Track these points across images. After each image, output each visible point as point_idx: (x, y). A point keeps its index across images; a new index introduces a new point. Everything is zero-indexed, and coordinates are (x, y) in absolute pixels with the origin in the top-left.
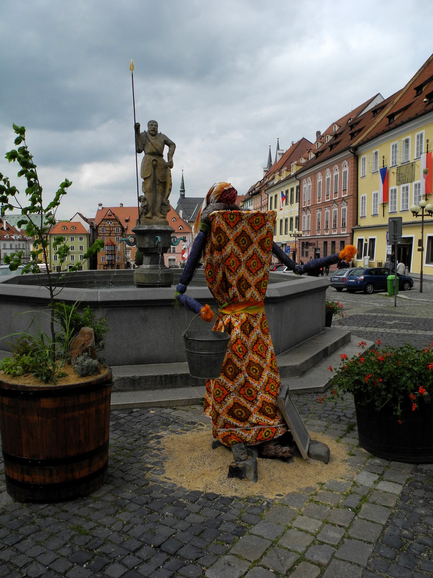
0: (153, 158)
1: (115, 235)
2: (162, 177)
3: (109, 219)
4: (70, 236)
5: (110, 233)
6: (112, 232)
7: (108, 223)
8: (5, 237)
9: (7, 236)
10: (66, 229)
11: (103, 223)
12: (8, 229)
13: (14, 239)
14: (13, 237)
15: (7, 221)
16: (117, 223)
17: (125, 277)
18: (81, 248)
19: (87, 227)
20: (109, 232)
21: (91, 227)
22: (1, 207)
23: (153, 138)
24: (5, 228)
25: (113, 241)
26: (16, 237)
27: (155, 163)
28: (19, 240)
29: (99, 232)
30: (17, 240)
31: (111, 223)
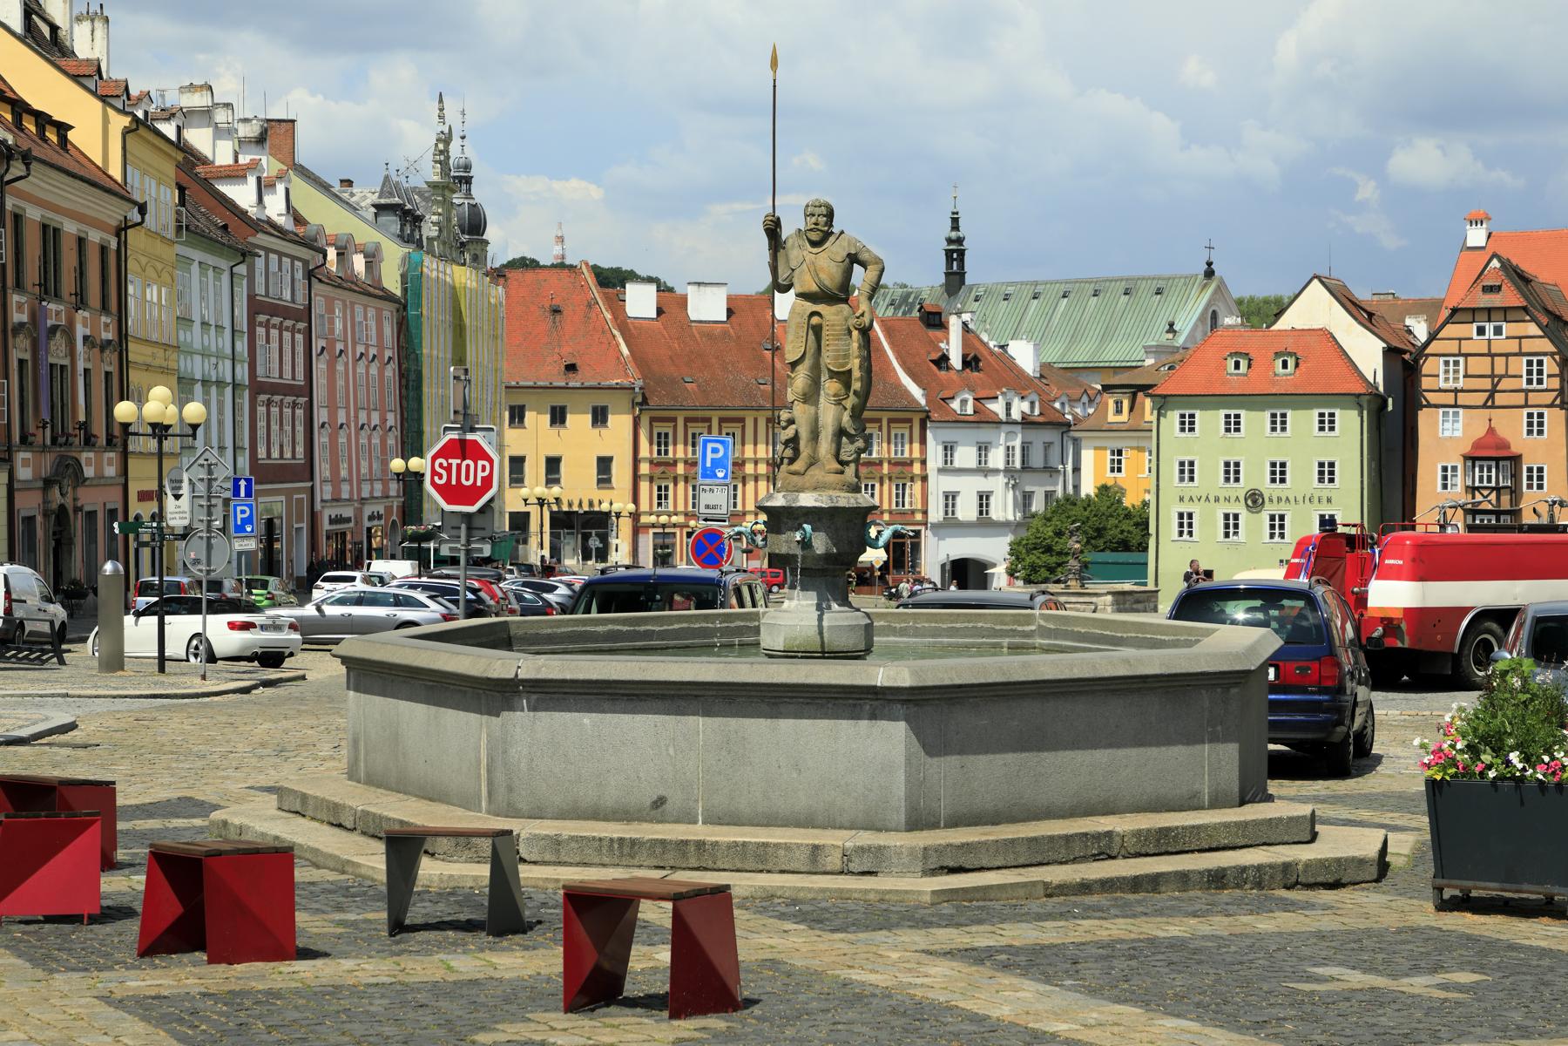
0: (810, 307)
1: (1519, 399)
2: (836, 358)
3: (1489, 312)
4: (1217, 407)
5: (1493, 392)
6: (1505, 384)
7: (1481, 331)
8: (955, 405)
9: (964, 402)
10: (1243, 364)
11: (1451, 330)
12: (970, 362)
13: (1003, 416)
14: (997, 407)
15: (966, 317)
16: (1533, 329)
17: (739, 631)
18: (1327, 472)
19: (1368, 353)
20: (1486, 384)
21: (1391, 353)
22: (950, 241)
23: (815, 250)
24: (956, 361)
25: (1503, 432)
26: (1008, 406)
27: (815, 320)
28: (1026, 422)
29: (1426, 383)
30: (1015, 423)
31: (1498, 331)
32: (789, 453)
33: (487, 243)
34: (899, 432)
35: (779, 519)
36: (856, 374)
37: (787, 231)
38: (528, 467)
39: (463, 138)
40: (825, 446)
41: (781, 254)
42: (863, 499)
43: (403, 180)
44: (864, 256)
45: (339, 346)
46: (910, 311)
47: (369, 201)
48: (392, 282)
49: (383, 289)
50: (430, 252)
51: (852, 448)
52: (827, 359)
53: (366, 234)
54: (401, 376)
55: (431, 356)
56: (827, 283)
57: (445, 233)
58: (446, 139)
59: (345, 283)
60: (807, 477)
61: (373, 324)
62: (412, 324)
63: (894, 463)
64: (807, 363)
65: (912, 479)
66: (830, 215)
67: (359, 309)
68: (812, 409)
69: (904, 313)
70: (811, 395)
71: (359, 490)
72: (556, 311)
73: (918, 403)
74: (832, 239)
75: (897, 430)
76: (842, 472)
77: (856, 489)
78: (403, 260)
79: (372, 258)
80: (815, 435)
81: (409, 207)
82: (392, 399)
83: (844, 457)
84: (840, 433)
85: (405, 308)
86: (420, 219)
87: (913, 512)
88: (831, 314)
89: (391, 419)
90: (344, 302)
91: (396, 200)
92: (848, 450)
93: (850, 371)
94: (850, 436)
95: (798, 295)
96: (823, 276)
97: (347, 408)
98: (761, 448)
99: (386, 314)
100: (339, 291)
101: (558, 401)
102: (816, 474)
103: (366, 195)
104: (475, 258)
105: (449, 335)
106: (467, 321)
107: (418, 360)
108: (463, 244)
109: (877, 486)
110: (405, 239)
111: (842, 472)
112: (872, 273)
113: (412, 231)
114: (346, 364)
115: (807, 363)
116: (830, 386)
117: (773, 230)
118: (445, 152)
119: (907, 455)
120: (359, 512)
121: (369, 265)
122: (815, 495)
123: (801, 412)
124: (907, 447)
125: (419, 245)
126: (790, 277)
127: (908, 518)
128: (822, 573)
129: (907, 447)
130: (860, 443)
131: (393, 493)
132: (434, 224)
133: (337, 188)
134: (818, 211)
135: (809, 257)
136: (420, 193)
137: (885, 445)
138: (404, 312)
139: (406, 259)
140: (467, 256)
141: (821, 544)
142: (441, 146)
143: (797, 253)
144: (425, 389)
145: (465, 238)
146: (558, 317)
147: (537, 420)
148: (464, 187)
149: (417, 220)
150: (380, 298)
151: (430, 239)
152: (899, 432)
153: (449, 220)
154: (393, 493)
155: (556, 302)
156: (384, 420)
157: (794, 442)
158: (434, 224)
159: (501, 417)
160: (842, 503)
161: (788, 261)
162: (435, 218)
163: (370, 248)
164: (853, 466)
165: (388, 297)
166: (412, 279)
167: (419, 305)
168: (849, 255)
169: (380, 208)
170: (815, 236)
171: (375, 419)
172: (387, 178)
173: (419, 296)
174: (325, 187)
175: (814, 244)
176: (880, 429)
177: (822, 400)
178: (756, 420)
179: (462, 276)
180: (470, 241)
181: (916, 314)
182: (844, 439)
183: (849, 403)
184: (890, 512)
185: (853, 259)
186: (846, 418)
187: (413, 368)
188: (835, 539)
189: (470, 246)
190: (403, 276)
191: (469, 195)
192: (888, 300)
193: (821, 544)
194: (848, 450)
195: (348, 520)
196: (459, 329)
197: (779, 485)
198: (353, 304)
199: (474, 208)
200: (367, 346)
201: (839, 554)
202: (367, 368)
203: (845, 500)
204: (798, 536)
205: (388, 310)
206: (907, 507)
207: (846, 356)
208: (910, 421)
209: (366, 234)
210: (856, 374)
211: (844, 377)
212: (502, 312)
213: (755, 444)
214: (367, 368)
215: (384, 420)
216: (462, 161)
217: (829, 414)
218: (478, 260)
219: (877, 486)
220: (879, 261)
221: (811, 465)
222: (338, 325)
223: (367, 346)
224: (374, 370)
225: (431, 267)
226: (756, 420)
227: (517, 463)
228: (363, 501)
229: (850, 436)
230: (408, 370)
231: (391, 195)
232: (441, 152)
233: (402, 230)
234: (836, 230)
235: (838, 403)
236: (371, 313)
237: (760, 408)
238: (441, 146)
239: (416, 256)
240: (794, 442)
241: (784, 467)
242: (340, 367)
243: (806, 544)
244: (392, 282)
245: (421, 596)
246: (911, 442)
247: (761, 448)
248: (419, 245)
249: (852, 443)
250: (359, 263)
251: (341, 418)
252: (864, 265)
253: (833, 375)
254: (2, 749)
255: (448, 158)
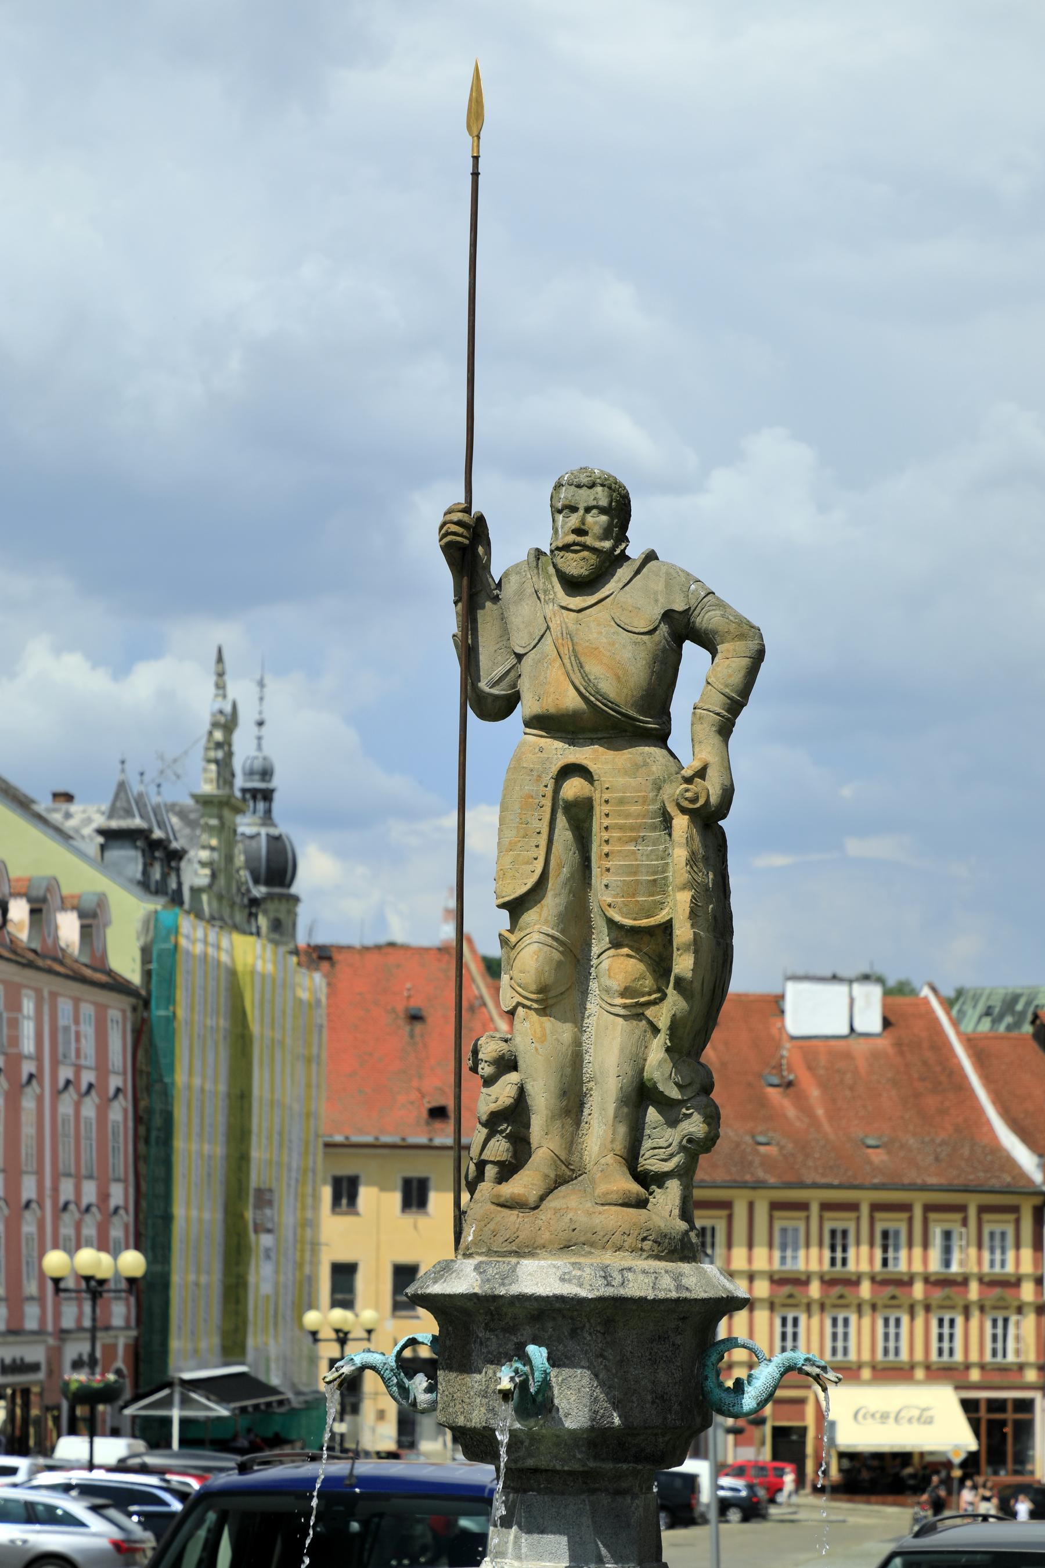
0: (560, 752)
2: (631, 890)
27: (574, 787)
32: (499, 1148)
33: (295, 899)
34: (998, 1228)
35: (473, 1329)
36: (683, 933)
37: (504, 557)
38: (361, 1281)
39: (260, 724)
40: (600, 1132)
41: (487, 615)
42: (702, 1280)
43: (152, 790)
44: (708, 619)
45: (28, 1067)
46: (1017, 1024)
47: (94, 825)
48: (125, 962)
49: (110, 973)
50: (197, 913)
51: (673, 1136)
52: (607, 895)
53: (80, 875)
54: (138, 1120)
55: (189, 1087)
56: (608, 687)
57: (222, 881)
58: (228, 723)
59: (42, 960)
60: (545, 1214)
61: (88, 1030)
62: (158, 1032)
63: (989, 1283)
64: (552, 904)
65: (1020, 1310)
66: (619, 510)
67: (65, 1006)
68: (565, 1032)
69: (1009, 1028)
70: (562, 993)
71: (57, 1315)
72: (415, 1018)
73: (1030, 1181)
74: (623, 573)
75: (994, 1224)
76: (641, 1204)
77: (685, 1249)
78: (146, 923)
79: (92, 920)
80: (572, 1102)
81: (158, 834)
82: (121, 1161)
83: (650, 1163)
84: (641, 1096)
85: (147, 1003)
86: (178, 855)
87: (1021, 1367)
88: (616, 771)
89: (117, 1194)
90: (38, 992)
91: (137, 822)
92: (663, 1142)
93: (667, 927)
94: (666, 1105)
95: (528, 724)
96: (595, 669)
97: (40, 1173)
98: (761, 1253)
99: (114, 1014)
100: (29, 973)
101: (416, 1171)
102: (571, 1206)
103: (89, 816)
104: (277, 926)
105: (223, 1053)
106: (255, 1028)
107: (167, 1094)
108: (254, 902)
109: (959, 1321)
110: (146, 886)
111: (641, 1204)
112: (731, 662)
113: (165, 876)
114: (40, 1099)
115: (552, 904)
116: (615, 968)
117: (466, 547)
118: (225, 746)
119: (1010, 1268)
120: (55, 1356)
121: (87, 932)
122: (562, 1263)
123: (536, 1039)
124: (1010, 1255)
125: (176, 899)
126: (512, 675)
127: (1012, 1378)
128: (585, 1482)
129: (1010, 1255)
130: (694, 1125)
131: (117, 1321)
132: (203, 864)
133: (43, 804)
134: (585, 497)
135: (560, 621)
136: (182, 814)
137: (973, 1251)
138: (144, 1012)
139: (151, 922)
140: (263, 921)
141: (577, 1400)
142: (218, 735)
143: (535, 611)
144: (179, 1144)
145: (260, 891)
146: (418, 1027)
147: (379, 1201)
148: (261, 806)
149: (173, 857)
150: (103, 986)
151: (196, 891)
152: (998, 1228)
153: (229, 858)
154: (117, 1321)
155: (416, 1003)
156: (104, 1196)
157: (513, 1118)
158: (203, 864)
159: (316, 1197)
160: (638, 1287)
161: (505, 633)
162: (204, 855)
163: (89, 904)
164: (674, 1186)
165: (118, 985)
166: (160, 956)
167: (170, 1000)
168: (668, 616)
169: (111, 837)
170: (576, 565)
171: (90, 1192)
172: (122, 786)
173: (169, 982)
174: (22, 803)
175: (574, 585)
176: (965, 1223)
177: (593, 1006)
178: (751, 1206)
179: (249, 953)
180: (269, 897)
181: (1028, 1029)
182: (652, 1114)
183: (662, 1015)
184: (982, 1367)
185: (681, 628)
186: (656, 1053)
187: (158, 1106)
188: (616, 1387)
189: (271, 906)
190: (146, 953)
191: (268, 818)
192: (981, 1008)
193: (577, 1400)
194: (663, 1142)
195: (35, 1367)
196: (241, 1042)
197: (469, 1236)
198: (54, 996)
199: (276, 842)
200: (78, 1069)
201: (628, 1428)
202: (77, 1106)
203: (648, 1279)
204: (505, 1378)
205: (117, 1010)
206: (1011, 1358)
207: (658, 886)
208: (1015, 1209)
209: (80, 875)
210: (683, 933)
211: (652, 943)
212: (321, 1016)
213: (750, 1245)
214: (77, 1106)
215: (104, 1196)
216: (258, 765)
217: (611, 1046)
218: (282, 928)
219: (959, 1321)
220: (749, 632)
221: (559, 1182)
222: (28, 1028)
223: (78, 1069)
224: (89, 1110)
225: (193, 936)
226: (751, 1206)
227: (344, 1274)
228: (63, 1334)
229: (666, 1105)
230: (149, 1111)
231: (129, 813)
232: (219, 745)
233: (145, 873)
234: (635, 550)
235: (636, 1013)
236: (87, 1010)
237: (758, 1185)
238: (218, 735)
239: (168, 916)
240: (513, 1118)
241: (485, 1188)
242: (28, 1104)
243: (532, 1401)
244: (125, 962)
245: (77, 1508)
246: (1018, 1246)
247: (761, 1253)
248: (176, 899)
249: (673, 1123)
250: (68, 928)
251: (28, 1189)
252: (708, 642)
253: (623, 936)
254: (722, 1566)
255: (230, 754)
